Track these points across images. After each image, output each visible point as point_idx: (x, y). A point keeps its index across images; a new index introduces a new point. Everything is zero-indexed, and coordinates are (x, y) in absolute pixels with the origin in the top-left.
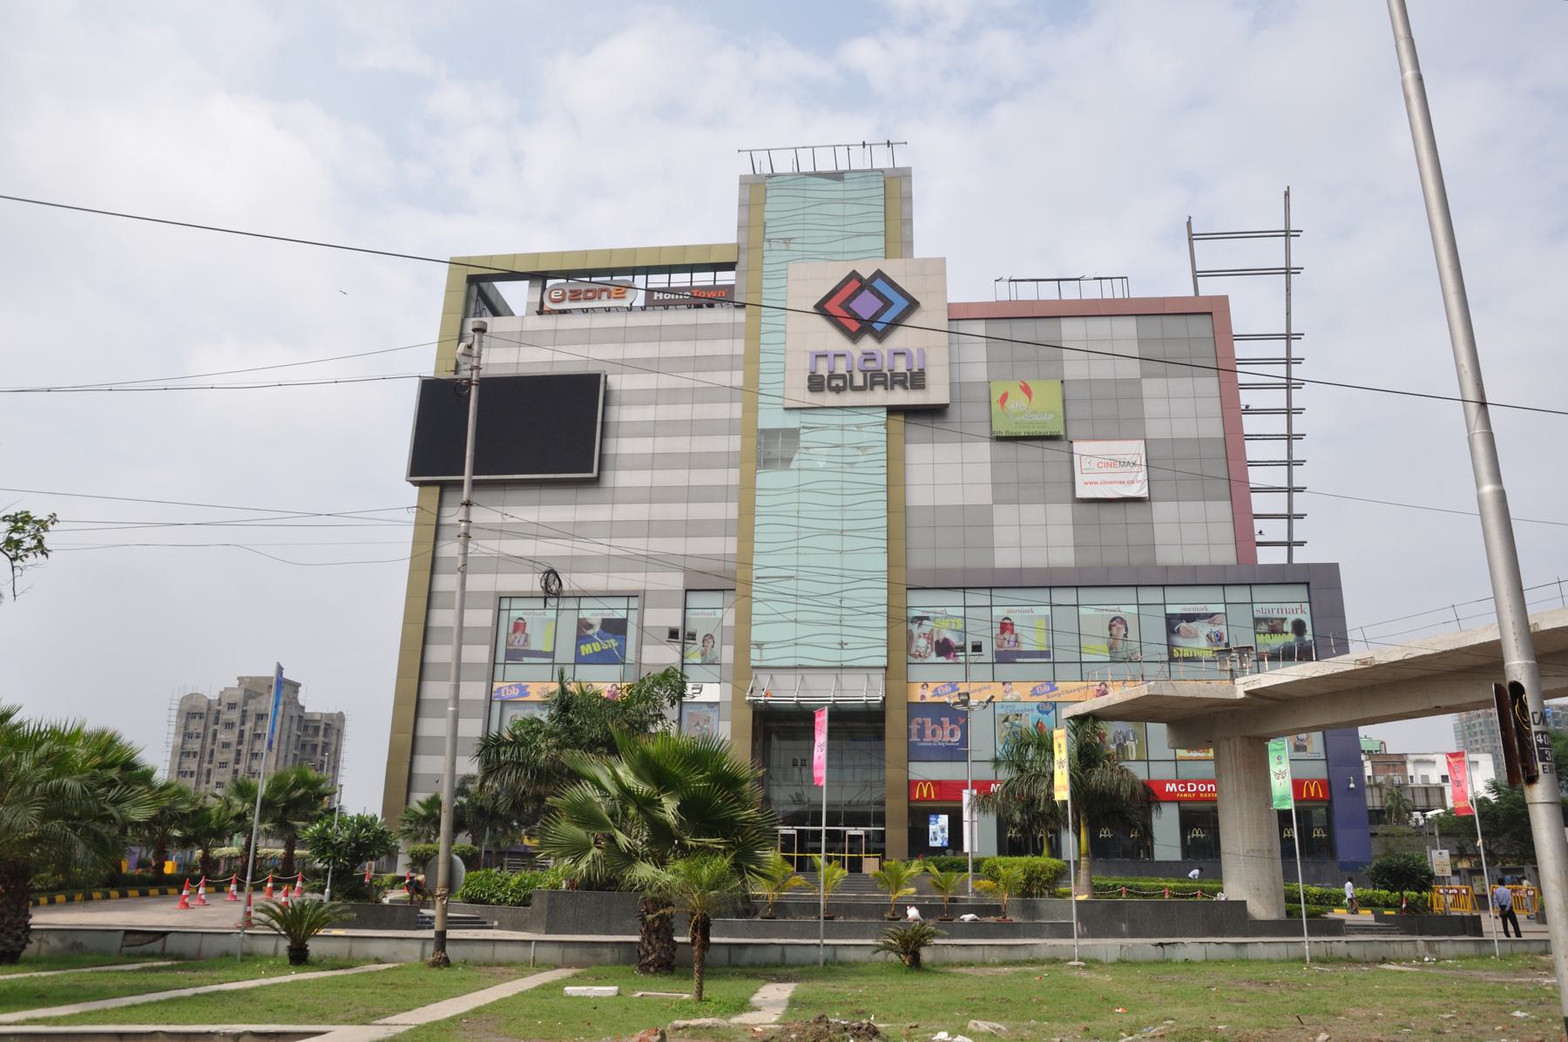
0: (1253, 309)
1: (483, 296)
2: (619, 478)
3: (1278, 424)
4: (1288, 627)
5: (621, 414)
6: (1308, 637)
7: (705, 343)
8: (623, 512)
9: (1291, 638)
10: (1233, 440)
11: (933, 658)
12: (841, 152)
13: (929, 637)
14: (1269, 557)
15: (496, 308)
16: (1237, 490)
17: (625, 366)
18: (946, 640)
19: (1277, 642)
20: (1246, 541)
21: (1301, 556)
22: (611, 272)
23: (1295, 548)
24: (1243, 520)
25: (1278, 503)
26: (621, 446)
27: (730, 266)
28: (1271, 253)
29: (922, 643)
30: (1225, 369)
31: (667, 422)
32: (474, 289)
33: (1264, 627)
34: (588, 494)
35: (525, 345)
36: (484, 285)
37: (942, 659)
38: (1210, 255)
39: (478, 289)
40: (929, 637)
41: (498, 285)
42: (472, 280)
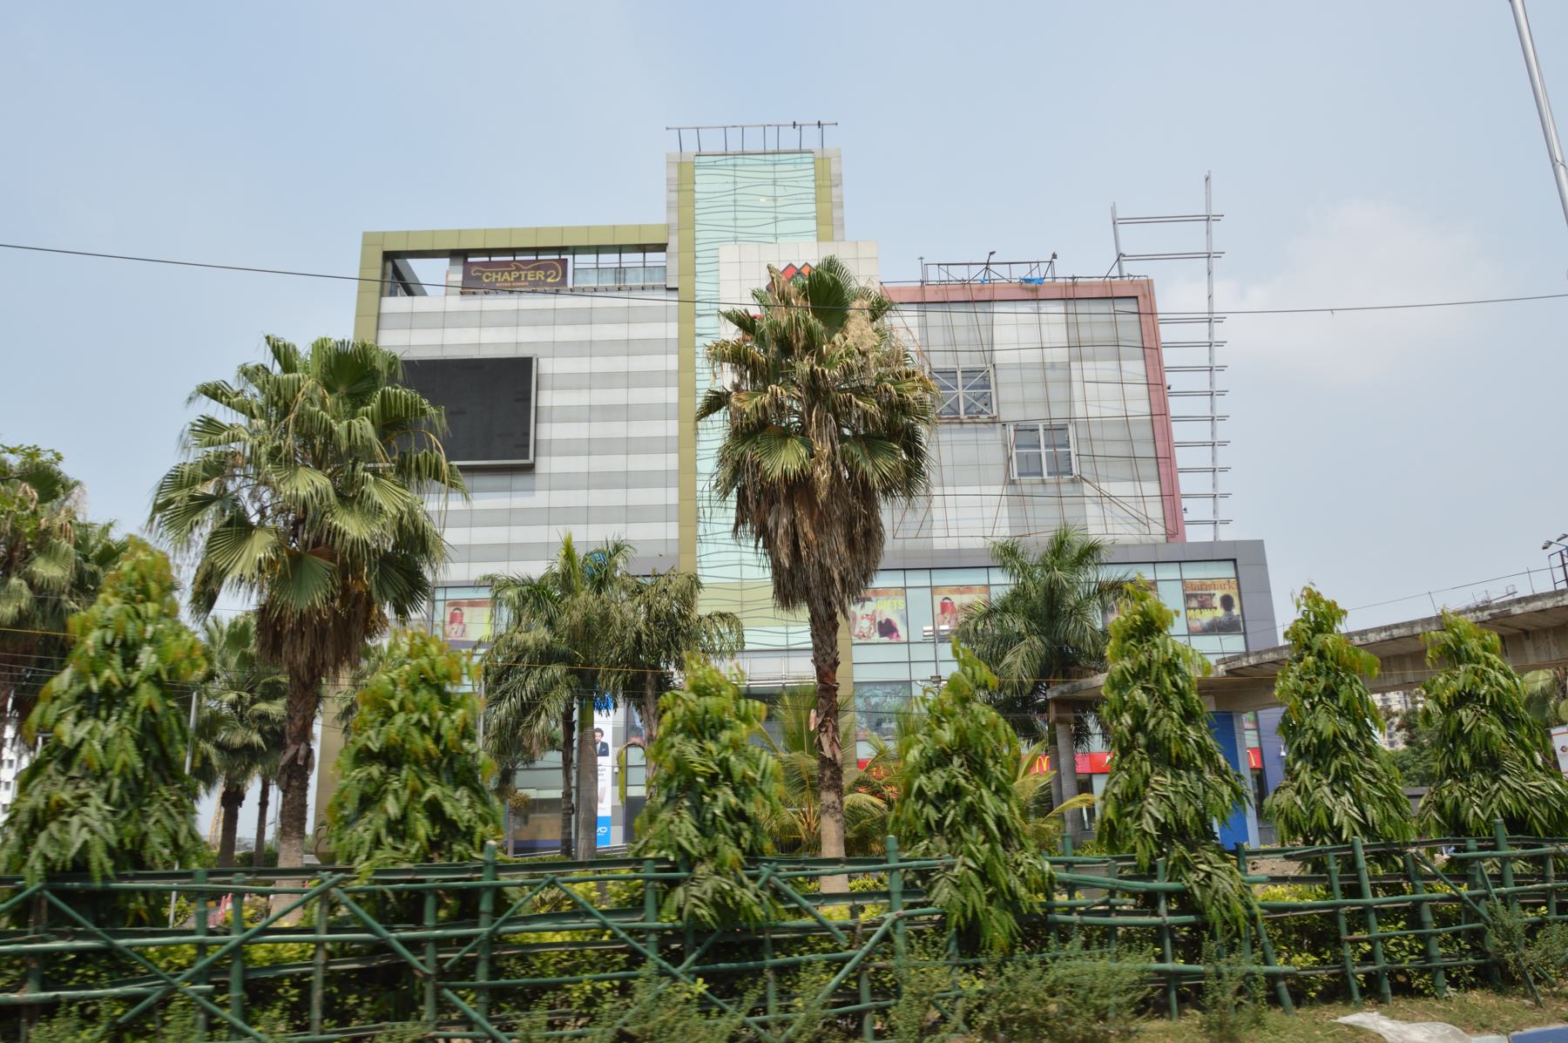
0: (1177, 294)
1: (397, 274)
2: (545, 465)
3: (1200, 357)
4: (1217, 602)
5: (546, 398)
6: (1236, 611)
7: (493, 330)
8: (560, 498)
9: (1220, 613)
10: (1160, 416)
11: (876, 637)
12: (771, 132)
13: (872, 618)
14: (1196, 535)
15: (408, 287)
16: (1164, 464)
17: (557, 349)
18: (888, 621)
19: (1206, 617)
20: (1174, 529)
21: (1227, 534)
22: (513, 251)
23: (1220, 500)
24: (1170, 497)
25: (1201, 431)
26: (546, 431)
27: (662, 248)
28: (1192, 237)
29: (866, 624)
30: (1151, 350)
31: (603, 407)
32: (389, 266)
33: (1194, 603)
34: (520, 480)
35: (444, 323)
36: (398, 262)
37: (886, 639)
38: (1133, 238)
39: (395, 270)
40: (872, 618)
41: (410, 261)
42: (389, 256)
